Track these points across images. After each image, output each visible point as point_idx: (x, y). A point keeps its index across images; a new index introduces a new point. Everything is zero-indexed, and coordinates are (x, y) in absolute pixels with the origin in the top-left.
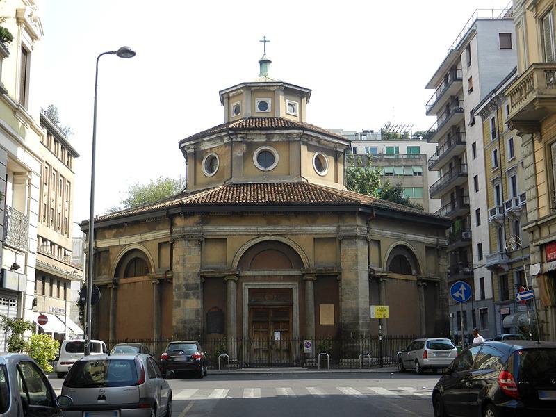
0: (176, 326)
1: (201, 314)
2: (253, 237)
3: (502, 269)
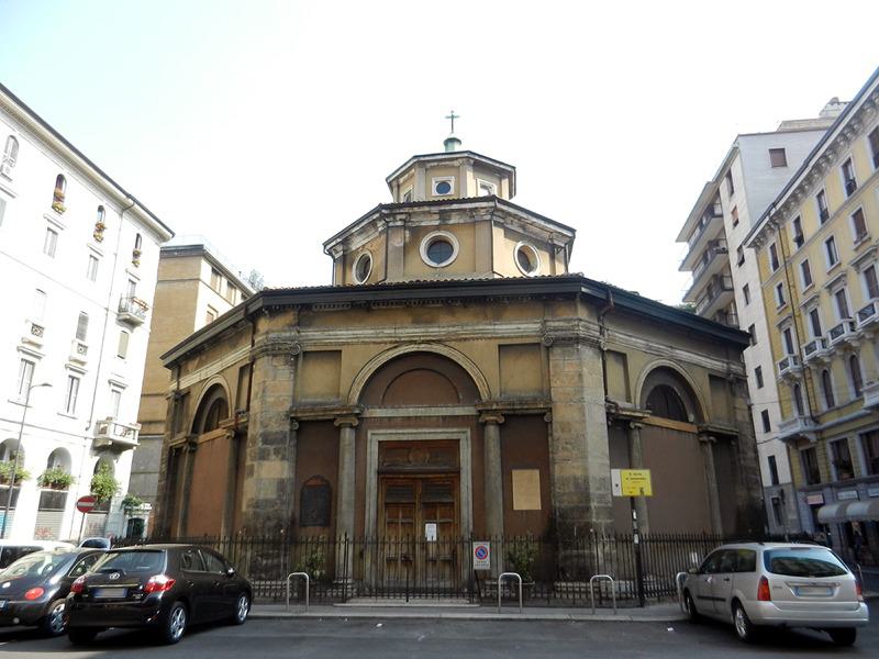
0: (245, 513)
1: (288, 490)
2: (389, 346)
3: (806, 440)
